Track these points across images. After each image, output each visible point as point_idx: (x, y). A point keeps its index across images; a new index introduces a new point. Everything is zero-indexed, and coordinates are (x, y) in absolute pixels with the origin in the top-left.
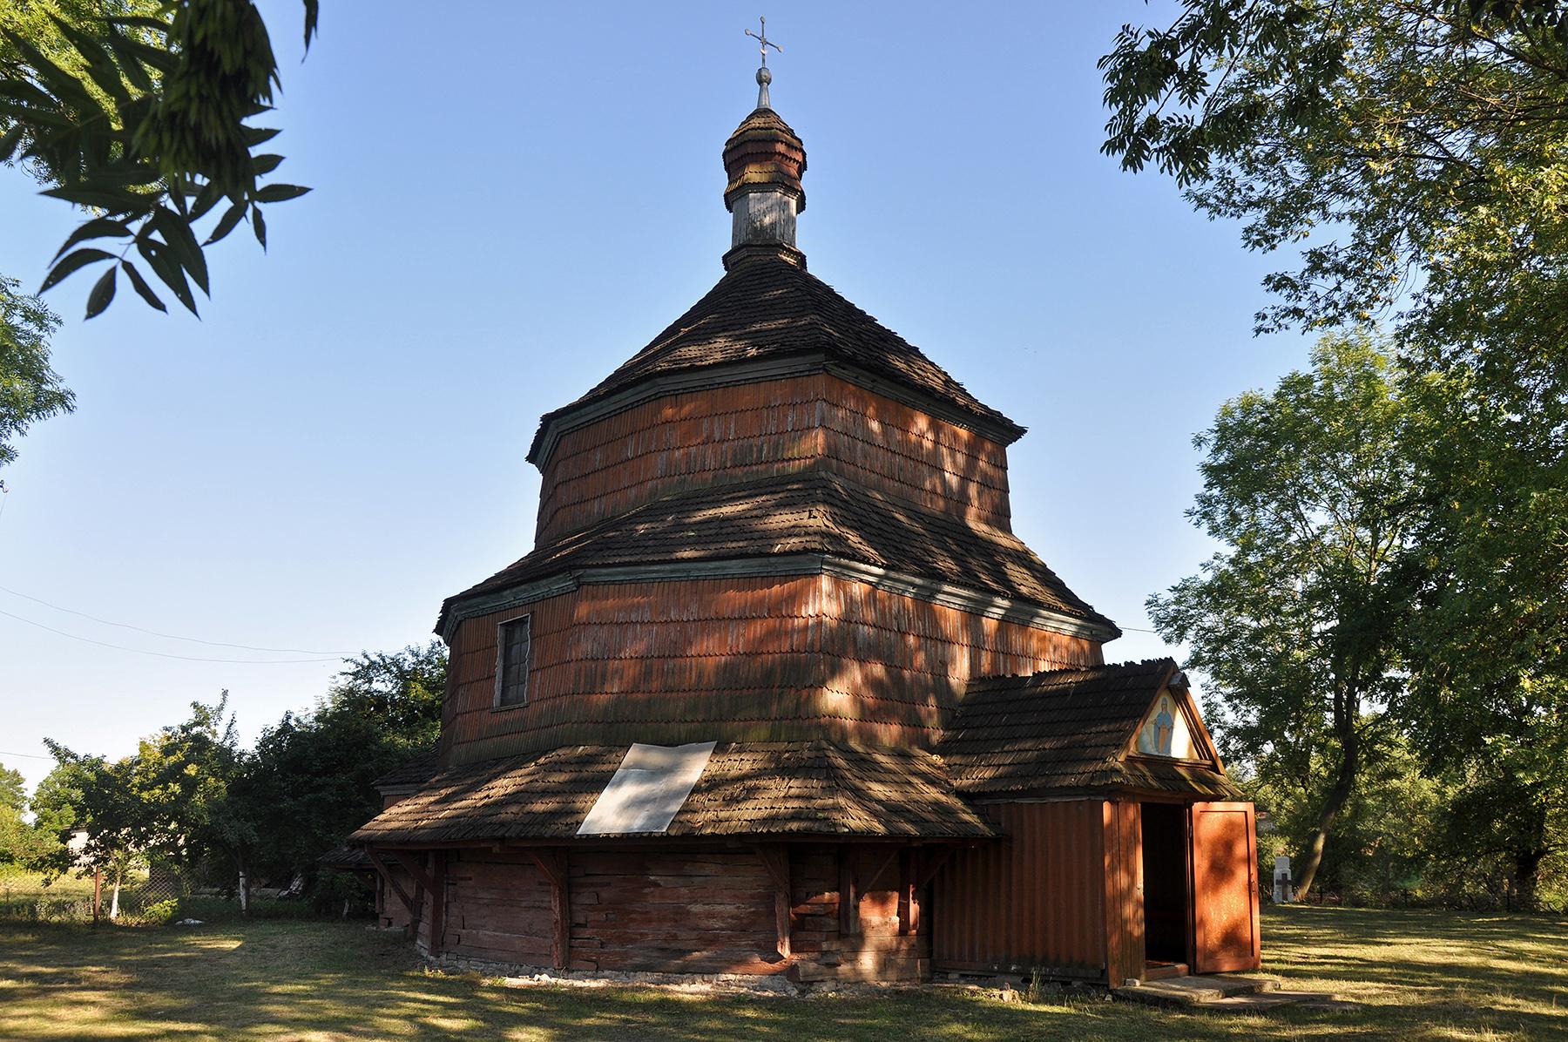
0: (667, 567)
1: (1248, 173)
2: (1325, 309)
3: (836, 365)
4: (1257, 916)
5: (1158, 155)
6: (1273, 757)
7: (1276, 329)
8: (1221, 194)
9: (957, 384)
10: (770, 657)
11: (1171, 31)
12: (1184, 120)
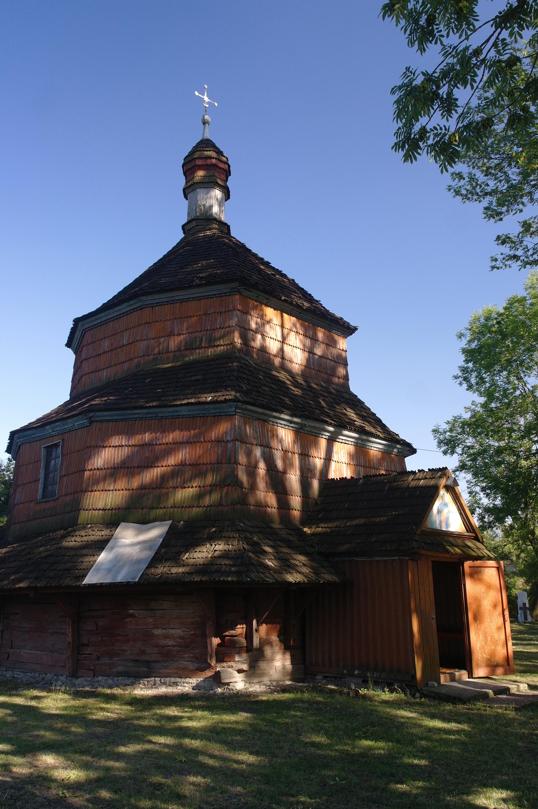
0: (144, 411)
1: (486, 175)
2: (532, 255)
3: (245, 289)
4: (508, 624)
5: (428, 149)
6: (511, 527)
7: (504, 267)
8: (469, 187)
9: (317, 301)
10: (205, 467)
11: (434, 72)
12: (443, 128)
